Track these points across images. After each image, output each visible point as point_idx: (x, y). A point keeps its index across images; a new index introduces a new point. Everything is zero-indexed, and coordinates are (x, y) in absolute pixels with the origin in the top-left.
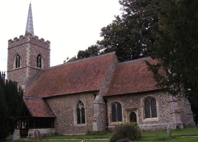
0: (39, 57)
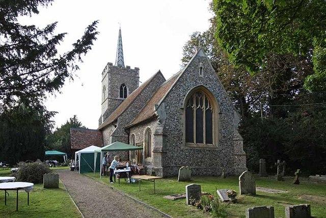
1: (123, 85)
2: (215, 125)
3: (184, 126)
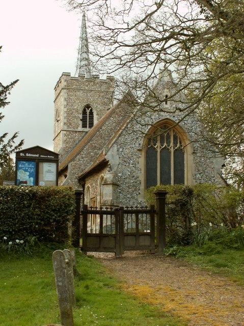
0: (88, 111)
1: (88, 106)
2: (187, 169)
3: (143, 172)
